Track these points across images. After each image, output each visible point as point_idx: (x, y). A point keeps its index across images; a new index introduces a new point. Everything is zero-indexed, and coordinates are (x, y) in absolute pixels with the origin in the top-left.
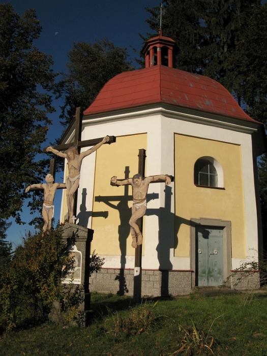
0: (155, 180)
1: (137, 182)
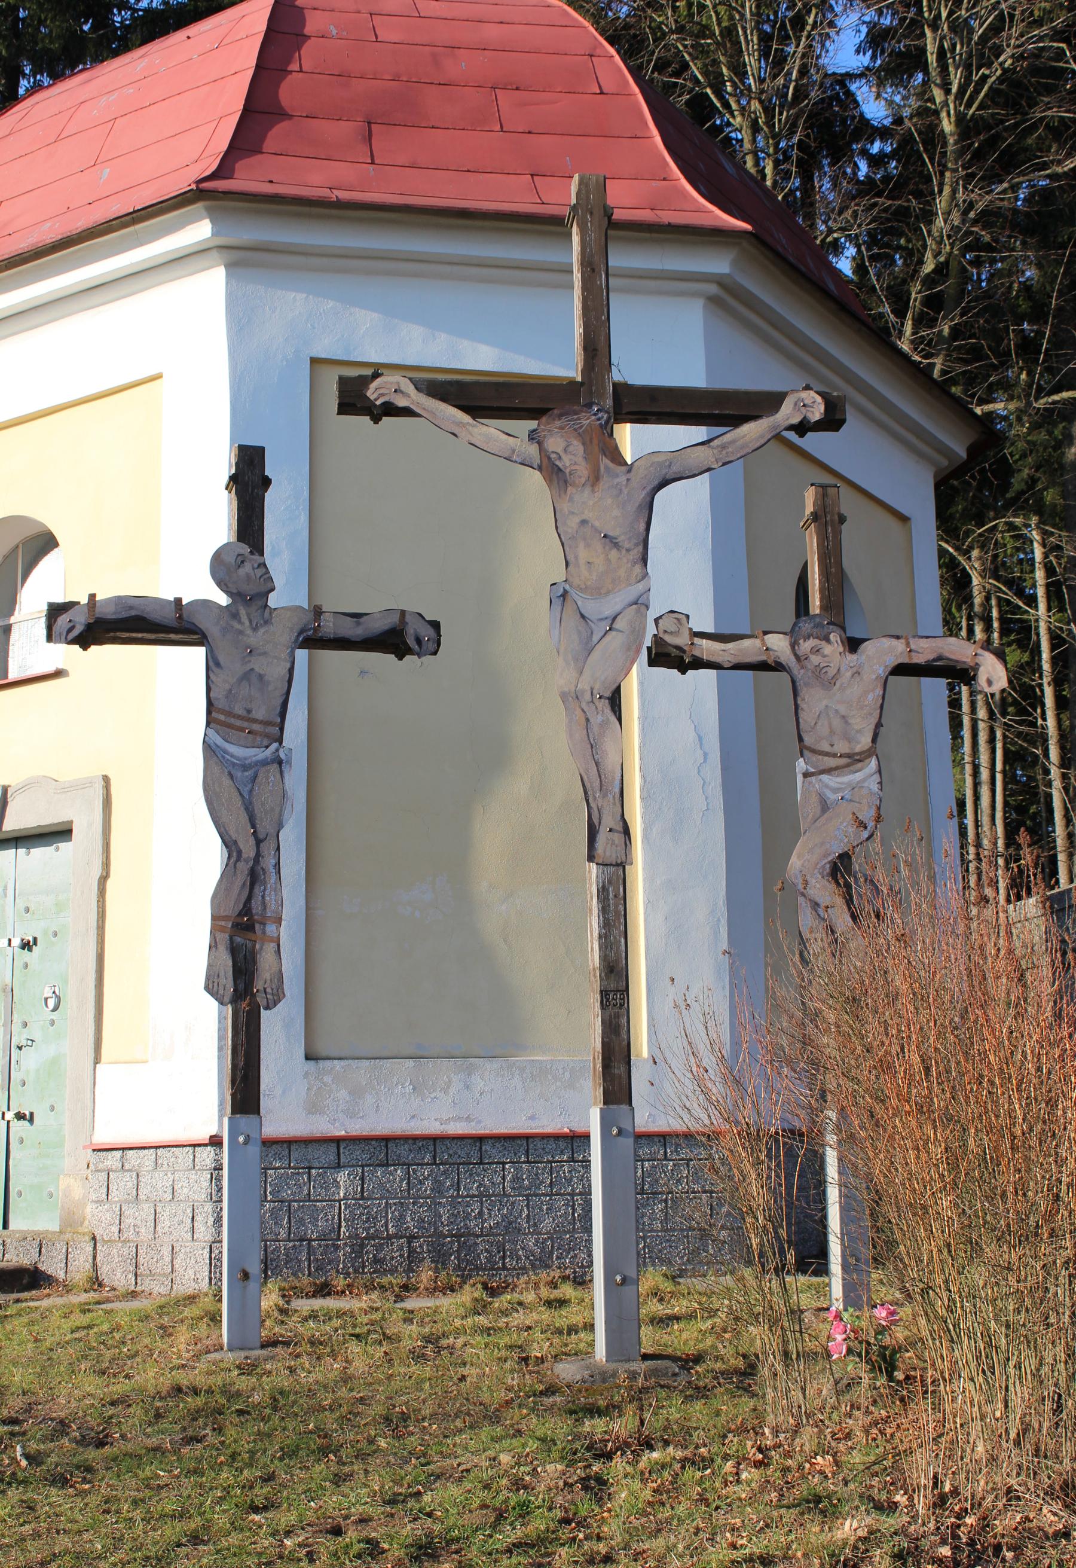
0: (919, 659)
1: (815, 659)
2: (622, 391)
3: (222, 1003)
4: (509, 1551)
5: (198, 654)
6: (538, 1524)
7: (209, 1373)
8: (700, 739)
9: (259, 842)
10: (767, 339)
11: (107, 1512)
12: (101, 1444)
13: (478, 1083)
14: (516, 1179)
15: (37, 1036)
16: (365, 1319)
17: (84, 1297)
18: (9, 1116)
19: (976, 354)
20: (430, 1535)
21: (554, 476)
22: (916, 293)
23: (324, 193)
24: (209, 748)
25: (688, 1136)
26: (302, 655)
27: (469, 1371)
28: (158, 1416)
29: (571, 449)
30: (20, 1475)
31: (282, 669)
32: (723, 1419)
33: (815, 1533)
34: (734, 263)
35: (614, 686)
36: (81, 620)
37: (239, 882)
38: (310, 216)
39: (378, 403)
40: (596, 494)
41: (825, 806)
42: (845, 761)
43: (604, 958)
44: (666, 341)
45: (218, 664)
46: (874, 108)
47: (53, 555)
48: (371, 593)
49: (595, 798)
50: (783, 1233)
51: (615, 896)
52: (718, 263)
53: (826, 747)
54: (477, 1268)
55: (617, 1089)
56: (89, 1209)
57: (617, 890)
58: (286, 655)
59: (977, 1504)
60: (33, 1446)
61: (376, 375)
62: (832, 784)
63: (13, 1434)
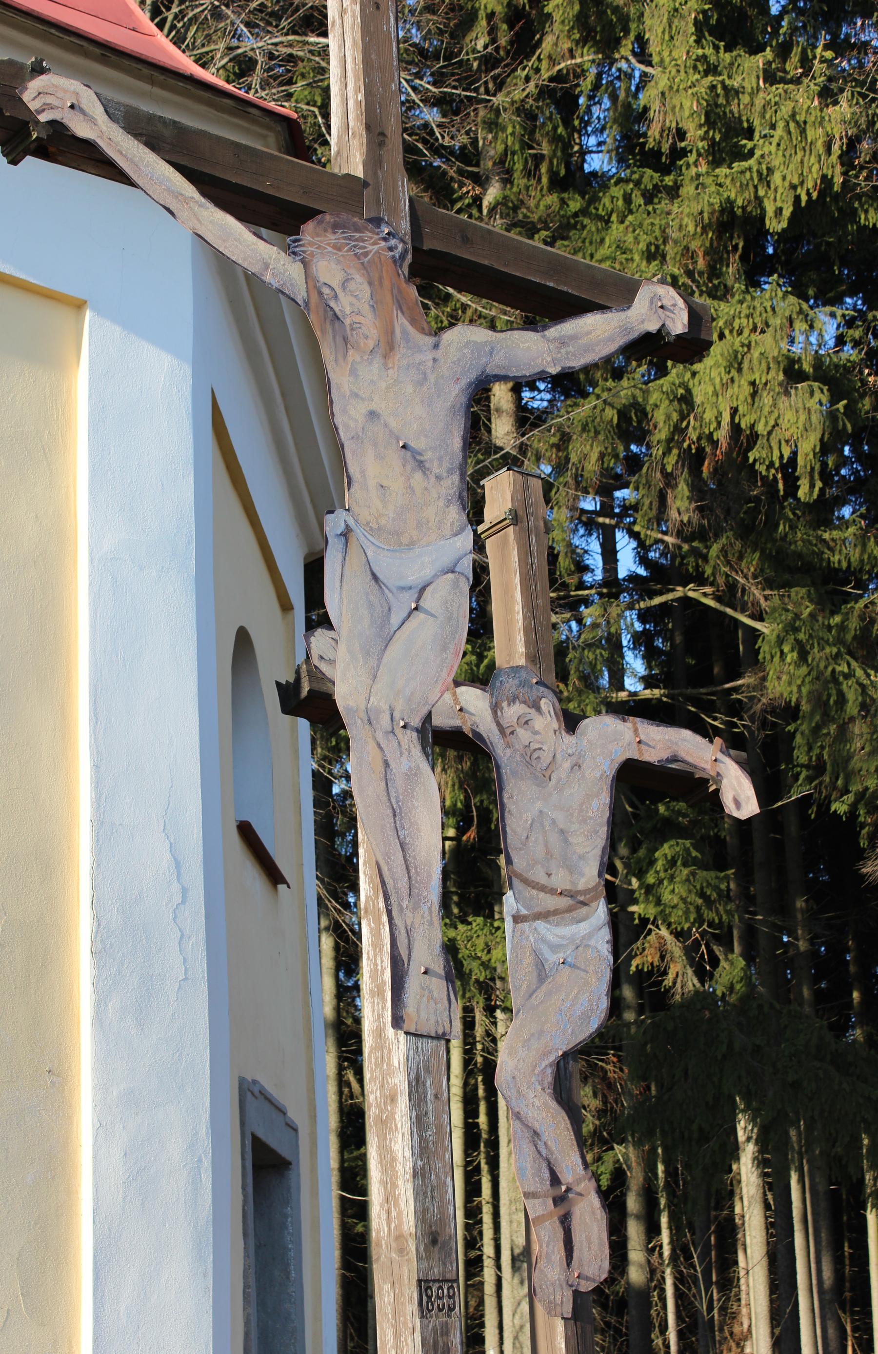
8: (178, 865)
21: (328, 327)
29: (352, 286)
35: (424, 712)
39: (43, 118)
40: (390, 372)
43: (422, 1215)
49: (401, 909)
51: (436, 1096)
53: (542, 879)
57: (437, 1084)
62: (550, 937)
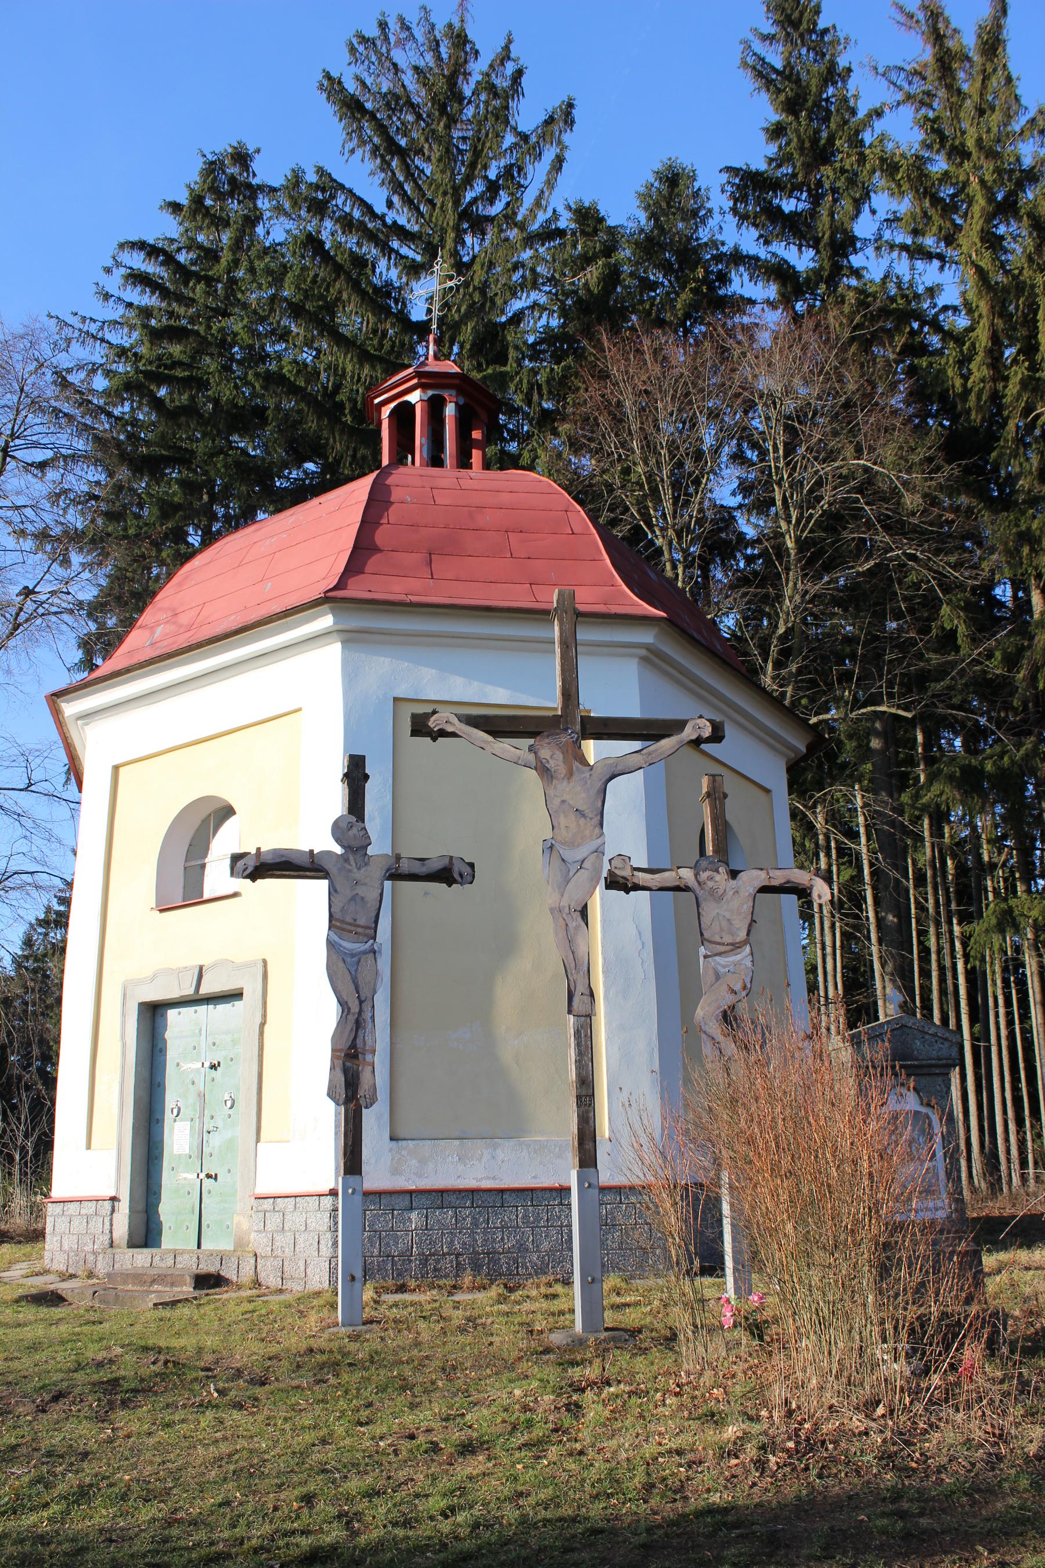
0: (775, 883)
1: (710, 884)
2: (586, 721)
3: (337, 1104)
4: (520, 1448)
5: (324, 884)
6: (538, 1432)
7: (330, 1340)
9: (361, 1002)
10: (678, 683)
11: (268, 1425)
12: (263, 1384)
13: (500, 1154)
14: (525, 1216)
15: (220, 1124)
16: (429, 1307)
17: (249, 1293)
18: (202, 1176)
19: (813, 683)
20: (470, 1439)
22: (774, 650)
23: (403, 597)
24: (330, 944)
25: (632, 1188)
26: (388, 884)
27: (496, 1339)
28: (299, 1367)
30: (214, 1403)
31: (376, 894)
32: (655, 1368)
33: (711, 1434)
34: (655, 637)
36: (251, 863)
37: (349, 1028)
38: (393, 611)
41: (718, 976)
42: (730, 948)
43: (578, 1075)
44: (615, 686)
45: (336, 891)
46: (748, 526)
47: (233, 819)
48: (431, 847)
50: (692, 1248)
52: (647, 637)
53: (718, 940)
54: (500, 1275)
55: (587, 1159)
56: (253, 1235)
58: (380, 883)
59: (811, 1417)
60: (221, 1385)
61: (434, 712)
63: (208, 1377)
